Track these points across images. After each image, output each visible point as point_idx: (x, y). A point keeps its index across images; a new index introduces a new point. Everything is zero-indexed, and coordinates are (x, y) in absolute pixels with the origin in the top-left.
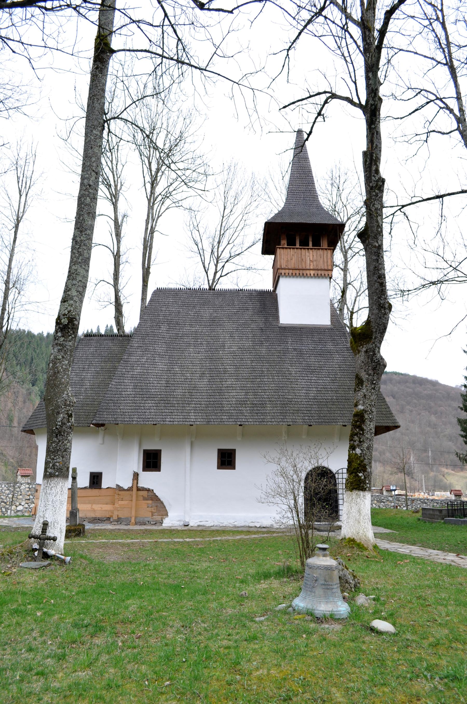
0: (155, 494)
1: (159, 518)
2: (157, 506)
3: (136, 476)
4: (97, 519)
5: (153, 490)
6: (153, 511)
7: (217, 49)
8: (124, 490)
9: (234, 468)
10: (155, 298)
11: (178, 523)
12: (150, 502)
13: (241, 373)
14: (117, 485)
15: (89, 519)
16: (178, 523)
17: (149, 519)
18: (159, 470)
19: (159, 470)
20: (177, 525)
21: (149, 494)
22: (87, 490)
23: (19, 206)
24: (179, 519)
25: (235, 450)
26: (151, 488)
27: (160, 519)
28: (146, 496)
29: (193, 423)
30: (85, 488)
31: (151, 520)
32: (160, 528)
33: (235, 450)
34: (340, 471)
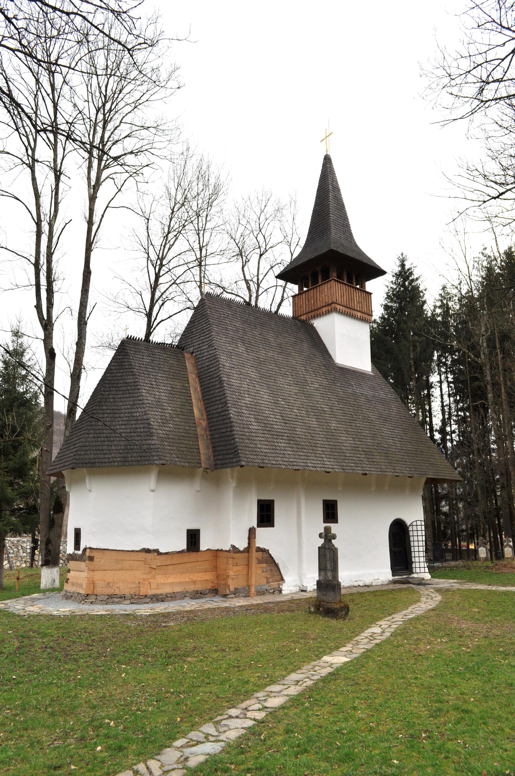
0: (270, 555)
1: (275, 584)
2: (271, 570)
3: (252, 532)
4: (199, 592)
5: (268, 550)
6: (268, 576)
7: (485, 52)
8: (239, 552)
9: (273, 526)
10: (118, 357)
11: (295, 588)
12: (264, 565)
13: (267, 431)
14: (233, 546)
15: (191, 593)
16: (295, 588)
17: (266, 587)
18: (273, 526)
19: (273, 526)
20: (294, 591)
21: (264, 556)
22: (184, 554)
23: (50, 211)
24: (295, 584)
25: (336, 501)
26: (267, 548)
27: (277, 586)
28: (261, 559)
29: (330, 470)
30: (182, 552)
31: (269, 588)
32: (277, 598)
33: (336, 501)
34: (415, 524)
